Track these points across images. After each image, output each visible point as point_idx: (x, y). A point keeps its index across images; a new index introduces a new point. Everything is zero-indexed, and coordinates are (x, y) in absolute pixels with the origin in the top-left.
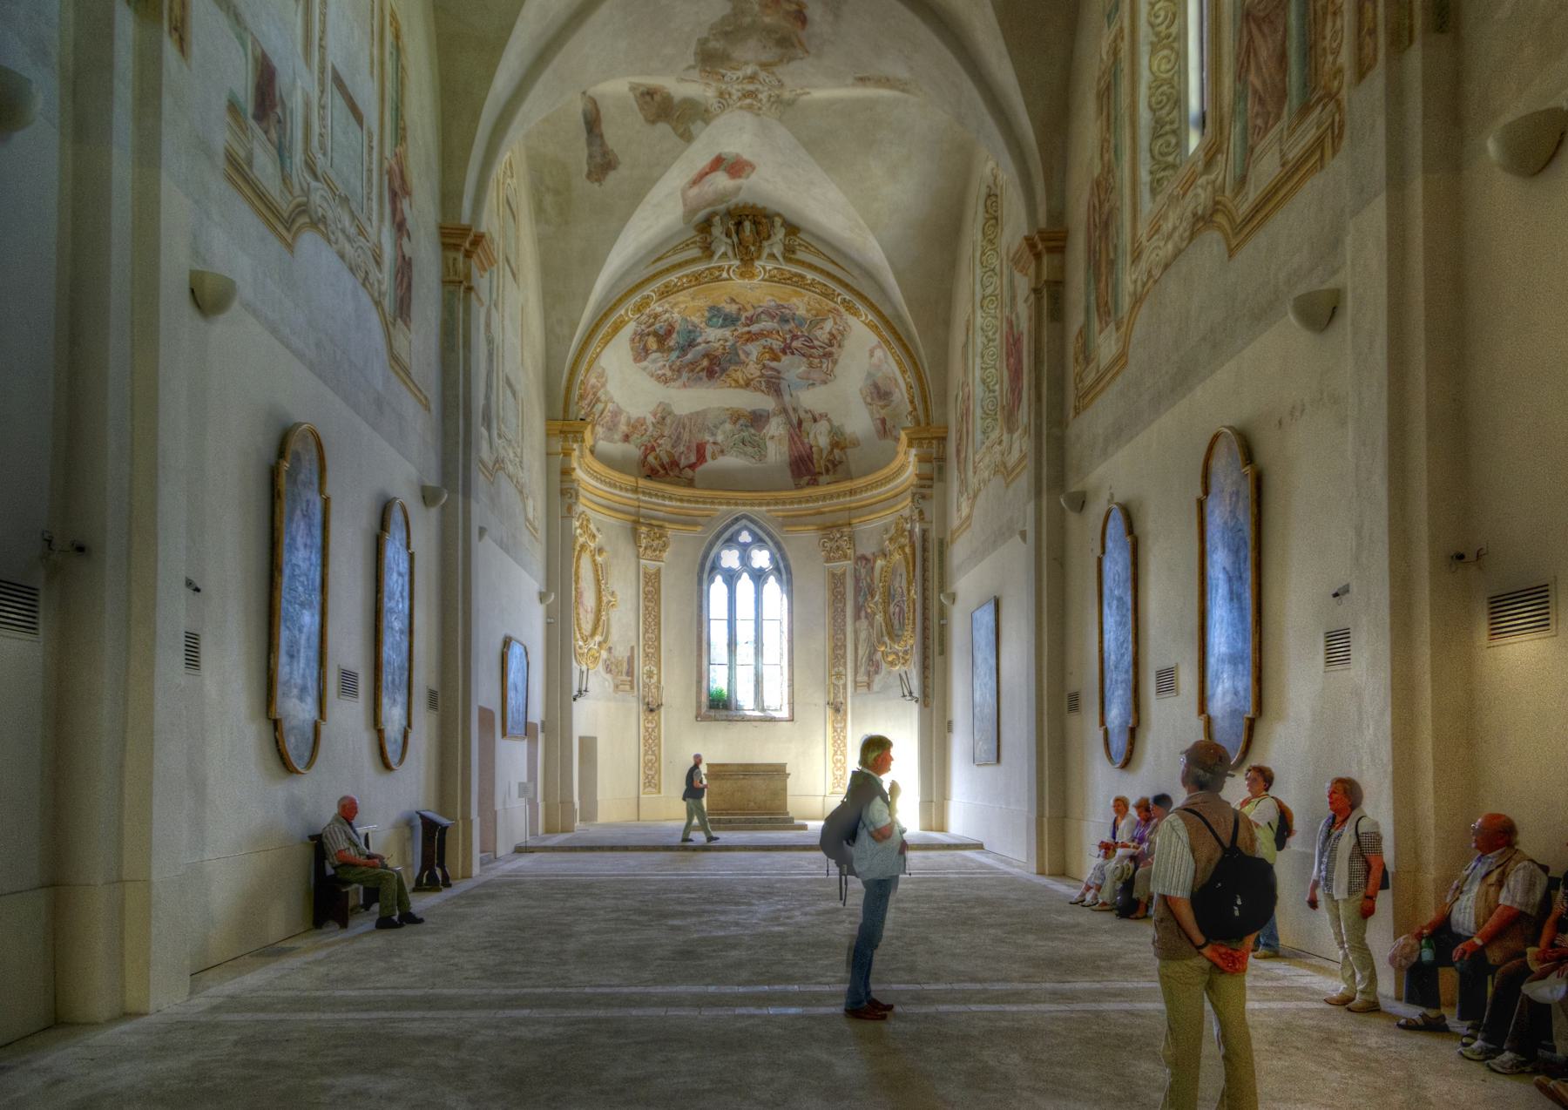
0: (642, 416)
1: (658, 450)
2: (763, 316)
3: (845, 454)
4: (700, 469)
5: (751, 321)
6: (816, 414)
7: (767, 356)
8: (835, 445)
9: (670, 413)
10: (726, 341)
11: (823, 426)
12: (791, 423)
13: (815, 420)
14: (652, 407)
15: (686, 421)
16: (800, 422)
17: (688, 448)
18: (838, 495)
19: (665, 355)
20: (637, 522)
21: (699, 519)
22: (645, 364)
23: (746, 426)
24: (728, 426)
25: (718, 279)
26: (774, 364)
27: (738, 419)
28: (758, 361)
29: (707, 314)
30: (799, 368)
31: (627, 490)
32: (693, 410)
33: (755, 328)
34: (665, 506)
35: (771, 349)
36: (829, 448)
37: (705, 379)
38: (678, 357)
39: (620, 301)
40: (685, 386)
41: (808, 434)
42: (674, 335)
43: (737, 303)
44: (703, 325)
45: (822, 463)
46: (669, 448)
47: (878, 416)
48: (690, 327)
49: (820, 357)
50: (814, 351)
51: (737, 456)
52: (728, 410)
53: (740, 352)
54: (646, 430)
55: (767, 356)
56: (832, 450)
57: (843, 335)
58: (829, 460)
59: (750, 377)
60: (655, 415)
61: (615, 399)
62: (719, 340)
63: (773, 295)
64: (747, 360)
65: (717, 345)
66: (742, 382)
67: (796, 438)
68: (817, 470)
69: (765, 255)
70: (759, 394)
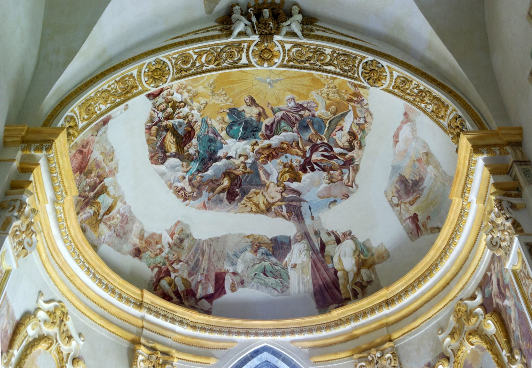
0: (158, 232)
1: (173, 275)
2: (283, 124)
3: (374, 272)
4: (217, 301)
5: (272, 131)
6: (340, 233)
7: (287, 176)
8: (361, 264)
9: (188, 236)
10: (247, 157)
11: (348, 245)
12: (312, 247)
13: (338, 241)
14: (170, 225)
15: (205, 247)
16: (323, 246)
17: (206, 277)
18: (372, 310)
19: (185, 164)
20: (135, 342)
21: (214, 352)
22: (162, 168)
23: (267, 255)
24: (249, 255)
25: (235, 65)
26: (294, 185)
27: (259, 247)
28: (279, 183)
29: (227, 119)
30: (319, 185)
31: (128, 301)
32: (212, 236)
33: (275, 141)
34: (174, 331)
35: (291, 167)
36: (355, 269)
37: (226, 201)
38: (199, 171)
39: (133, 60)
40: (204, 207)
41: (332, 258)
42: (194, 141)
43: (257, 106)
44: (223, 134)
45: (349, 287)
46: (185, 276)
47: (408, 216)
48: (211, 135)
49: (341, 167)
50: (334, 161)
51: (258, 288)
52: (248, 237)
53: (261, 172)
54: (161, 250)
55: (287, 176)
56: (359, 270)
57: (363, 130)
58: (356, 284)
59: (271, 201)
60: (172, 235)
61: (127, 200)
62: (240, 156)
63: (291, 91)
64: (268, 182)
65: (238, 162)
66: (262, 207)
67: (319, 265)
68: (344, 297)
69: (284, 30)
70: (280, 220)
